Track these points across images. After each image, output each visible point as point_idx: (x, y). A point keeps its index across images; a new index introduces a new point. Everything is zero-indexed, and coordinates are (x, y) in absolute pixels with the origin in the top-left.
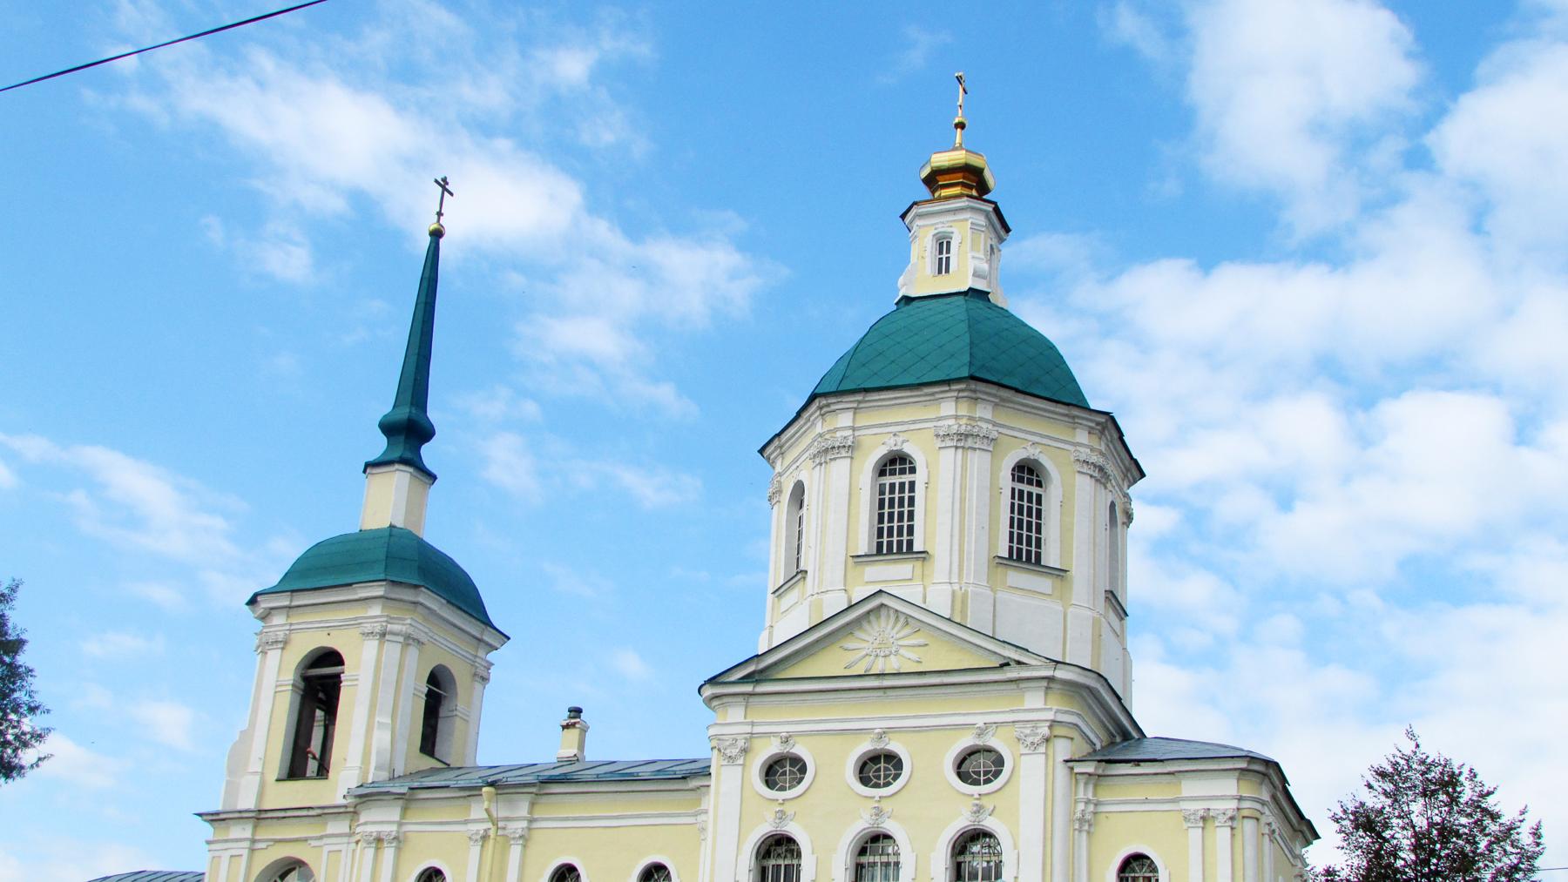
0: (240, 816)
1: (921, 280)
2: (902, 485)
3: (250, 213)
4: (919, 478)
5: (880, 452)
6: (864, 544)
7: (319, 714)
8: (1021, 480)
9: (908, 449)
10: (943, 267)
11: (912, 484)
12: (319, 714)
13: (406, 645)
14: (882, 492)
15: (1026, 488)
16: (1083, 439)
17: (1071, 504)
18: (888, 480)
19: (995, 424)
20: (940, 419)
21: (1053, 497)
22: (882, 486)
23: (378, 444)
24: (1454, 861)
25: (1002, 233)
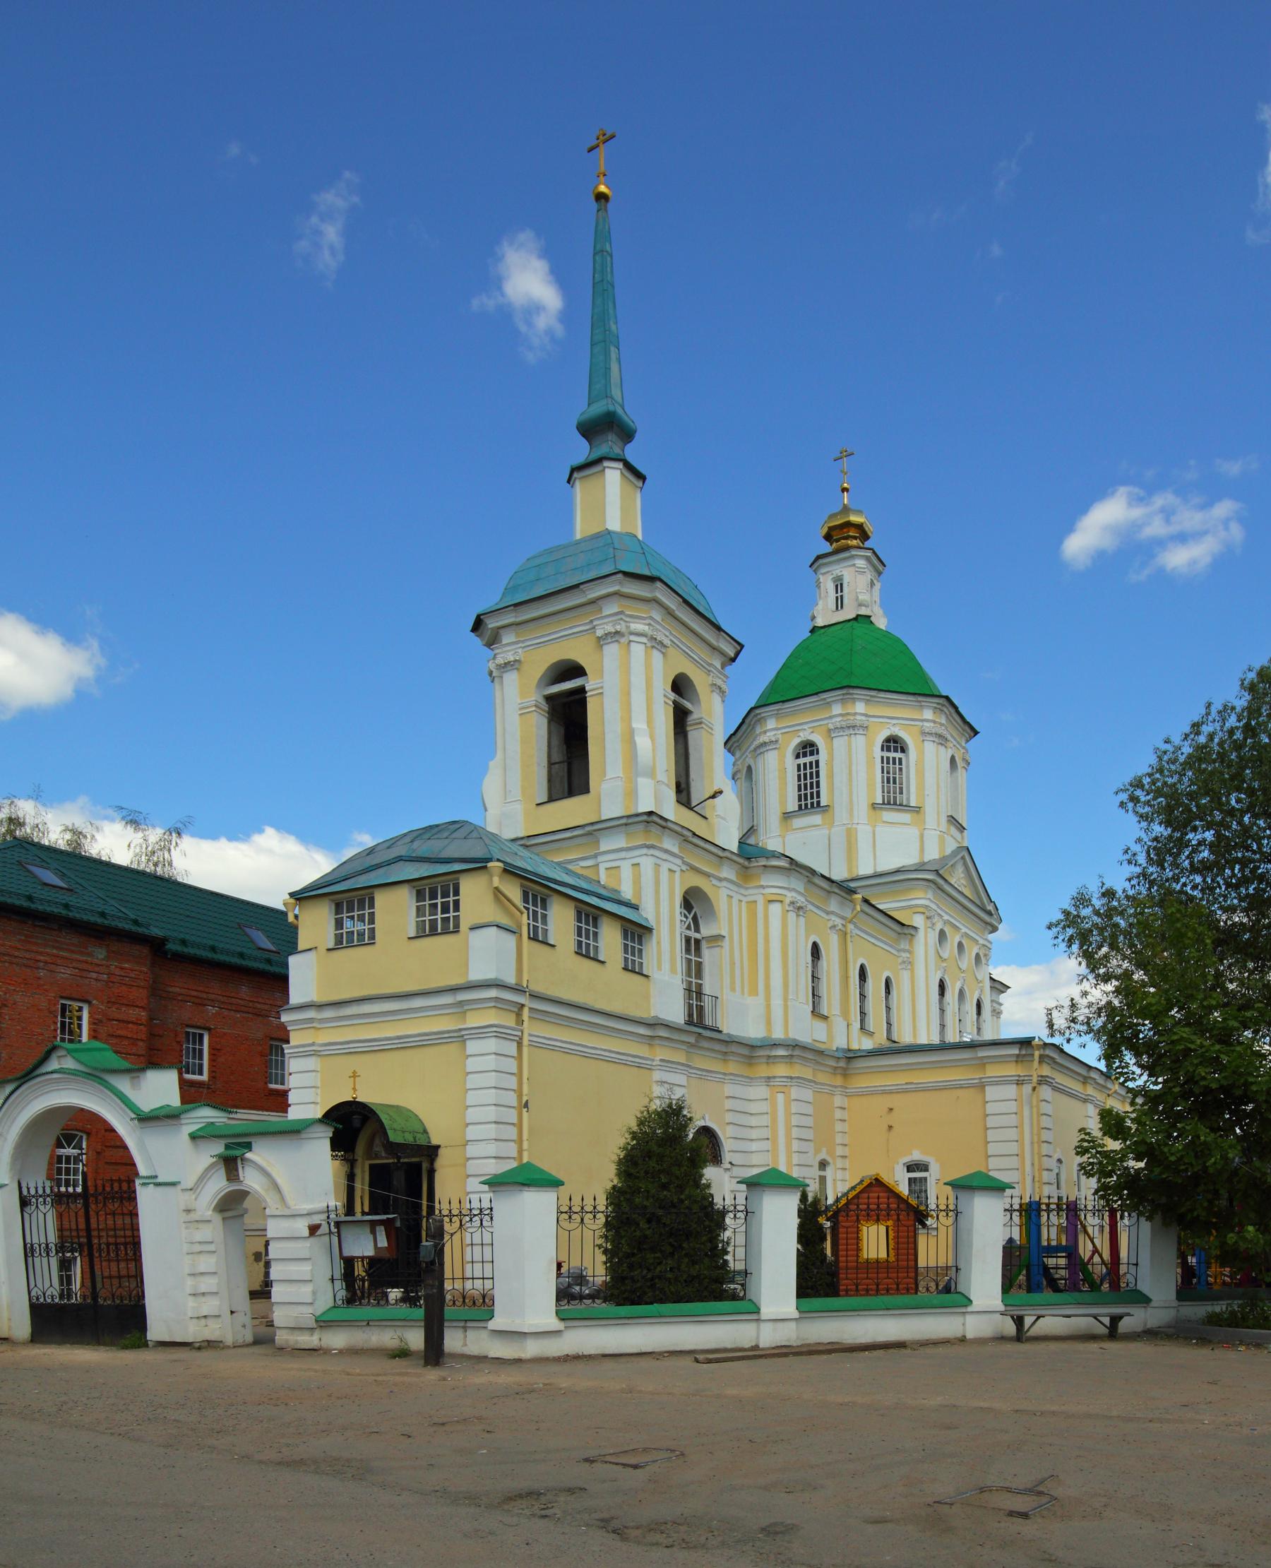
1: (825, 614)
2: (811, 763)
3: (1011, 1240)
4: (823, 757)
5: (885, 734)
6: (792, 805)
7: (612, 349)
8: (889, 750)
10: (840, 602)
11: (817, 762)
12: (612, 349)
14: (799, 770)
15: (892, 755)
16: (927, 714)
18: (802, 761)
19: (866, 715)
20: (831, 717)
22: (799, 766)
25: (881, 568)
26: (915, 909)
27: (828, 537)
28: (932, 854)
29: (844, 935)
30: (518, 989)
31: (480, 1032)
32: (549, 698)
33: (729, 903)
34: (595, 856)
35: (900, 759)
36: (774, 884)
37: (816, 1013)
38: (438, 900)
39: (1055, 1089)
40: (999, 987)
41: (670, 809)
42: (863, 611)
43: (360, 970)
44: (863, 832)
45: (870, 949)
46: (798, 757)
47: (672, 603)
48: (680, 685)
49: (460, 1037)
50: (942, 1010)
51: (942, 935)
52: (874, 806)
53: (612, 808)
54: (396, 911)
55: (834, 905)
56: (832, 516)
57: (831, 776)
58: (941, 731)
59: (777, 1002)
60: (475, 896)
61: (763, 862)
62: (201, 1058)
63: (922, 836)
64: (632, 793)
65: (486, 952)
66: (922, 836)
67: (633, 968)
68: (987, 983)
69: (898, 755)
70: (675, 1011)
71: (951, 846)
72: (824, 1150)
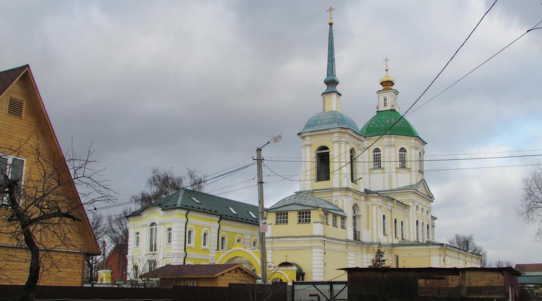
0: (421, 166)
4: (382, 153)
9: (379, 147)
10: (385, 105)
13: (346, 144)
15: (402, 153)
16: (412, 141)
17: (412, 155)
18: (375, 153)
21: (408, 154)
23: (324, 87)
24: (71, 199)
26: (410, 200)
28: (414, 182)
29: (391, 211)
30: (324, 237)
31: (316, 247)
32: (318, 154)
33: (362, 205)
36: (374, 200)
37: (384, 234)
38: (304, 217)
39: (450, 257)
40: (434, 218)
41: (351, 185)
42: (393, 108)
43: (282, 230)
44: (394, 175)
45: (398, 214)
46: (374, 152)
47: (351, 132)
48: (352, 151)
49: (311, 248)
50: (417, 229)
51: (417, 206)
52: (397, 168)
53: (336, 185)
54: (293, 217)
55: (389, 203)
58: (417, 146)
59: (375, 233)
60: (315, 215)
61: (371, 195)
64: (340, 182)
65: (316, 228)
67: (343, 227)
68: (430, 217)
69: (404, 153)
70: (351, 237)
71: (419, 179)
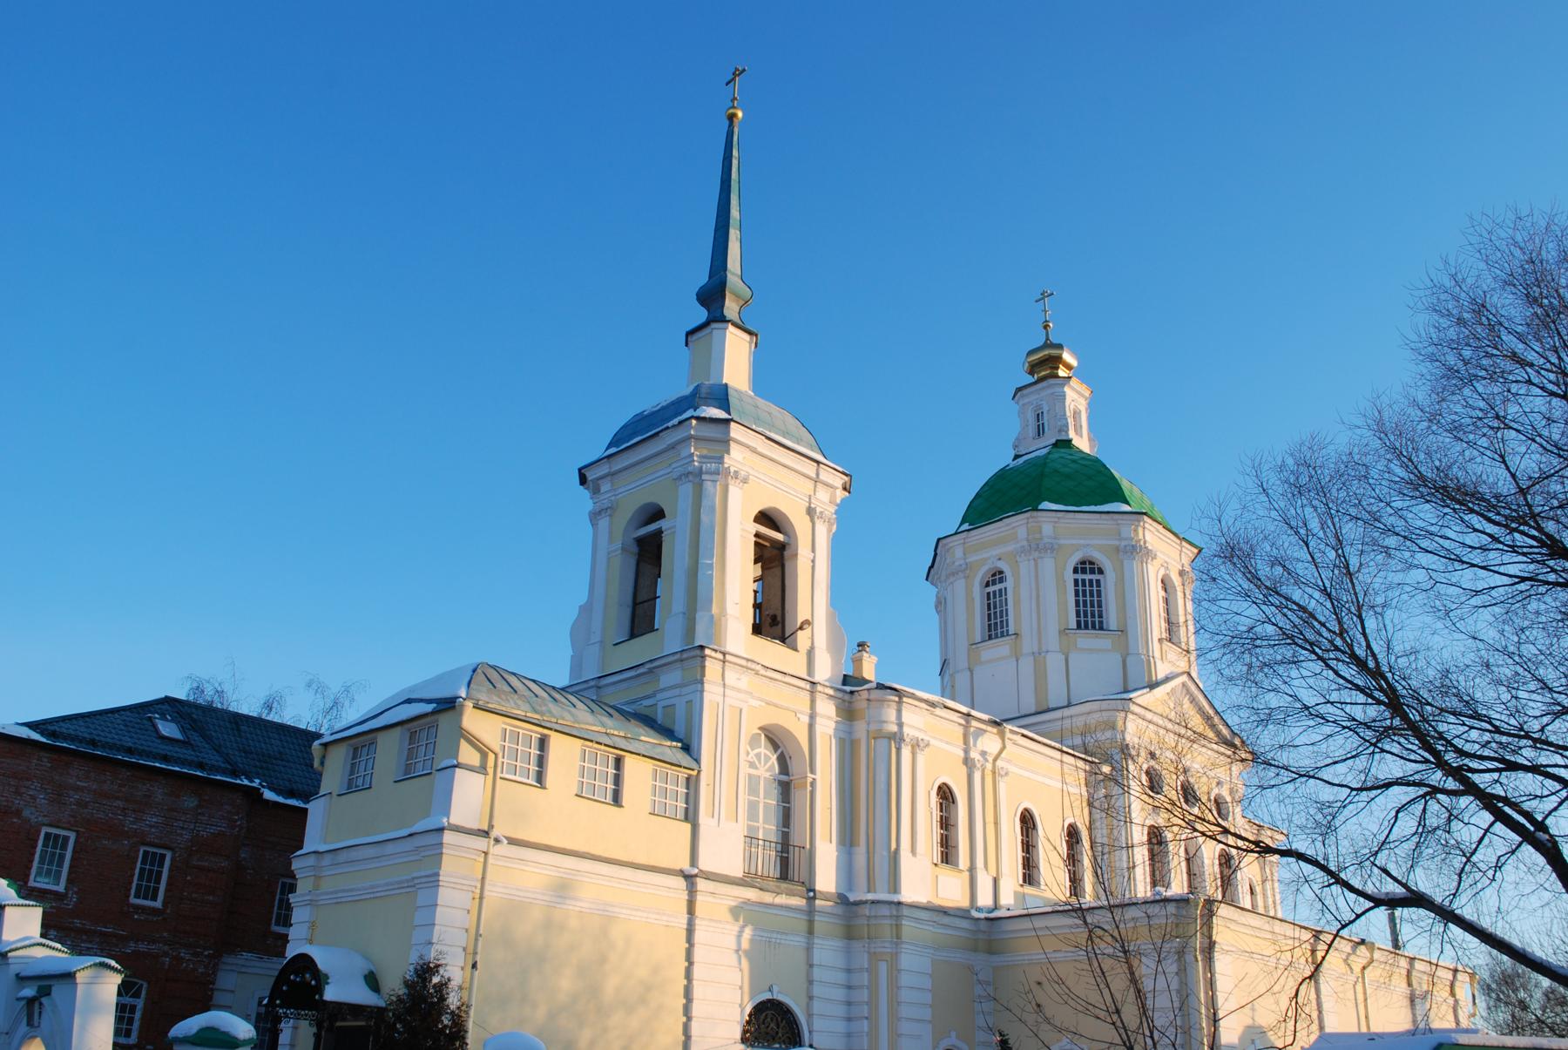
4: (1009, 584)
15: (1087, 577)
27: (1031, 373)
34: (653, 695)
35: (1098, 581)
56: (1030, 353)
57: (1017, 603)
62: (158, 881)
63: (1124, 662)
66: (1124, 662)
69: (1095, 577)
72: (953, 1034)
